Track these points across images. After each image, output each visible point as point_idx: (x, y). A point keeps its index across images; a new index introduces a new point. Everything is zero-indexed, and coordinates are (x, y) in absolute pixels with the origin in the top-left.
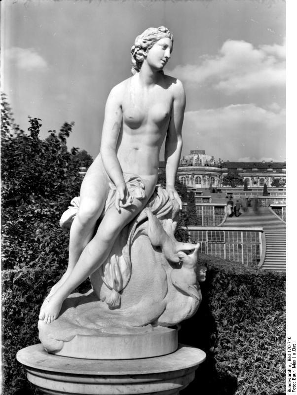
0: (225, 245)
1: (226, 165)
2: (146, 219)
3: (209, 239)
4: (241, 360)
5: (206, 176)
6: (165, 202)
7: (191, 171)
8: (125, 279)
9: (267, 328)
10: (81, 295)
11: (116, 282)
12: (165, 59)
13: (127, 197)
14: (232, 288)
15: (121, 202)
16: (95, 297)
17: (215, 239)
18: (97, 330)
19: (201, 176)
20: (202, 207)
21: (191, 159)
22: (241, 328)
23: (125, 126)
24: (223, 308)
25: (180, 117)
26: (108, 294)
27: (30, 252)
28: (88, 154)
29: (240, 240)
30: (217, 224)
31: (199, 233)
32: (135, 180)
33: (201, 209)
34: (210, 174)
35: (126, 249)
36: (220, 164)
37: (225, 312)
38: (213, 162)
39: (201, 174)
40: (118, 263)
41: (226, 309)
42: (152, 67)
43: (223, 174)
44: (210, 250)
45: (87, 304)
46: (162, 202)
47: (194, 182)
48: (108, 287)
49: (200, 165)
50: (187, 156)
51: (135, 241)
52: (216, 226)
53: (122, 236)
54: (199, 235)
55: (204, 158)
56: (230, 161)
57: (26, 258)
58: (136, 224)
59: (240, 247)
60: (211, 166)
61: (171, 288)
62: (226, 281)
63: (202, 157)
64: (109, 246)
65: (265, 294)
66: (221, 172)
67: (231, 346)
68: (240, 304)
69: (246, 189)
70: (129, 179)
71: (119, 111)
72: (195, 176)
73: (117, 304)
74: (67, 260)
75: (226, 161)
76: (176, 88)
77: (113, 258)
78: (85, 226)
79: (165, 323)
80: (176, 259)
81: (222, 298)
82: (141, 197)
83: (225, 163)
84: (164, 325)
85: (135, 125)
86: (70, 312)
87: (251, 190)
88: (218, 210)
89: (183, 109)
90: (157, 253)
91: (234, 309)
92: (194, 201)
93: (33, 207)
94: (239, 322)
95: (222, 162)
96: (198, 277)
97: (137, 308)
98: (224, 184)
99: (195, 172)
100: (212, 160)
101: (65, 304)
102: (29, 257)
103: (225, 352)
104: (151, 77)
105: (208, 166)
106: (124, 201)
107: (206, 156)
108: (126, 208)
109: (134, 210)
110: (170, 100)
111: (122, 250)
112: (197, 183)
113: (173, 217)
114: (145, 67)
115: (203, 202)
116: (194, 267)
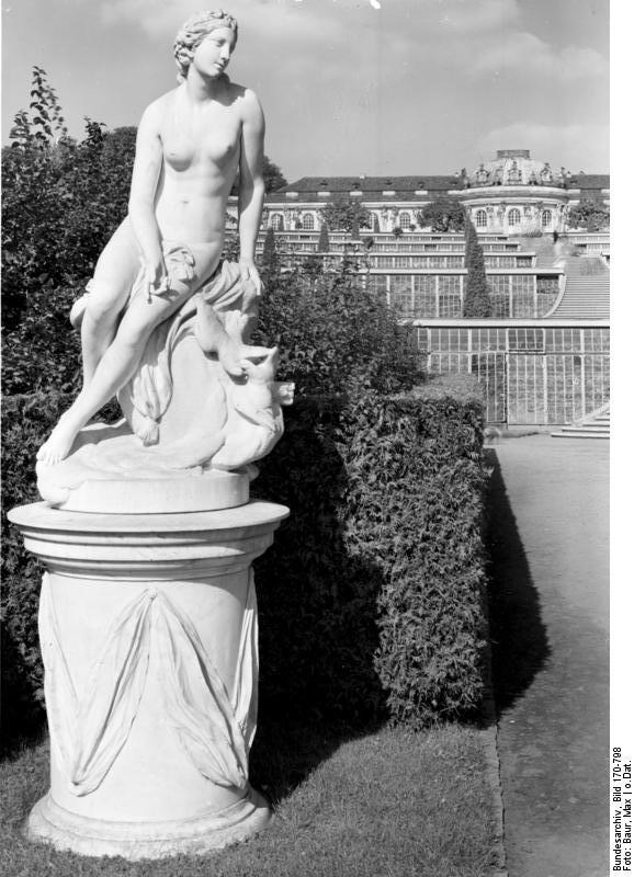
0: (545, 357)
1: (576, 182)
2: (194, 313)
3: (512, 346)
4: (397, 540)
5: (532, 207)
6: (229, 284)
7: (497, 196)
8: (164, 401)
9: (442, 487)
10: (107, 426)
11: (149, 405)
12: (222, 62)
13: (161, 279)
14: (385, 422)
15: (152, 286)
16: (127, 429)
17: (523, 346)
18: (118, 474)
19: (521, 208)
20: (511, 278)
21: (498, 170)
22: (399, 487)
23: (168, 167)
24: (370, 455)
26: (141, 422)
27: (62, 368)
28: (270, 163)
29: (579, 348)
30: (542, 313)
31: (491, 334)
32: (179, 252)
33: (507, 282)
34: (540, 203)
35: (163, 356)
36: (562, 181)
37: (374, 461)
38: (548, 177)
39: (520, 204)
40: (151, 379)
41: (376, 457)
42: (204, 75)
43: (571, 202)
44: (513, 369)
45: (118, 438)
46: (224, 286)
47: (506, 221)
48: (142, 414)
49: (518, 182)
50: (489, 164)
51: (179, 345)
52: (539, 318)
53: (158, 334)
54: (457, 342)
55: (528, 168)
57: (55, 378)
58: (178, 319)
59: (578, 361)
60: (542, 185)
61: (233, 415)
62: (375, 411)
63: (522, 164)
64: (136, 351)
65: (439, 431)
66: (567, 198)
67: (383, 517)
68: (398, 448)
70: (169, 250)
71: (157, 143)
72: (508, 208)
73: (154, 438)
76: (245, 103)
77: (145, 368)
78: (99, 323)
79: (221, 465)
80: (238, 372)
81: (367, 439)
82: (185, 277)
84: (221, 467)
85: (182, 165)
86: (87, 450)
88: (544, 284)
89: (261, 135)
90: (210, 363)
91: (388, 457)
92: (482, 264)
93: (70, 292)
94: (397, 477)
95: (569, 176)
96: (276, 398)
97: (186, 442)
98: (571, 224)
99: (507, 200)
100: (546, 170)
101: (79, 441)
102: (60, 376)
103: (374, 526)
104: (204, 88)
105: (536, 184)
106: (157, 285)
108: (161, 295)
109: (173, 298)
110: (235, 125)
111: (157, 356)
112: (511, 224)
113: (244, 308)
114: (192, 72)
115: (518, 267)
116: (267, 381)
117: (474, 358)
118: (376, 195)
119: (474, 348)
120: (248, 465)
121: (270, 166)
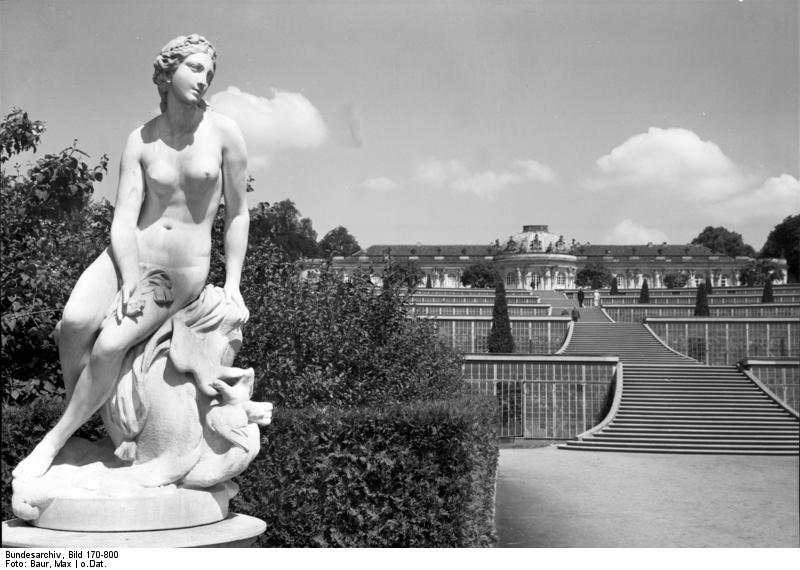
25: (144, 333)
54: (477, 372)
55: (546, 239)
56: (592, 243)
63: (543, 237)
69: (614, 291)
74: (251, 247)
75: (583, 243)
83: (582, 246)
87: (624, 293)
107: (550, 235)
117: (499, 385)
118: (429, 259)
119: (499, 377)
120: (226, 482)
121: (347, 236)
